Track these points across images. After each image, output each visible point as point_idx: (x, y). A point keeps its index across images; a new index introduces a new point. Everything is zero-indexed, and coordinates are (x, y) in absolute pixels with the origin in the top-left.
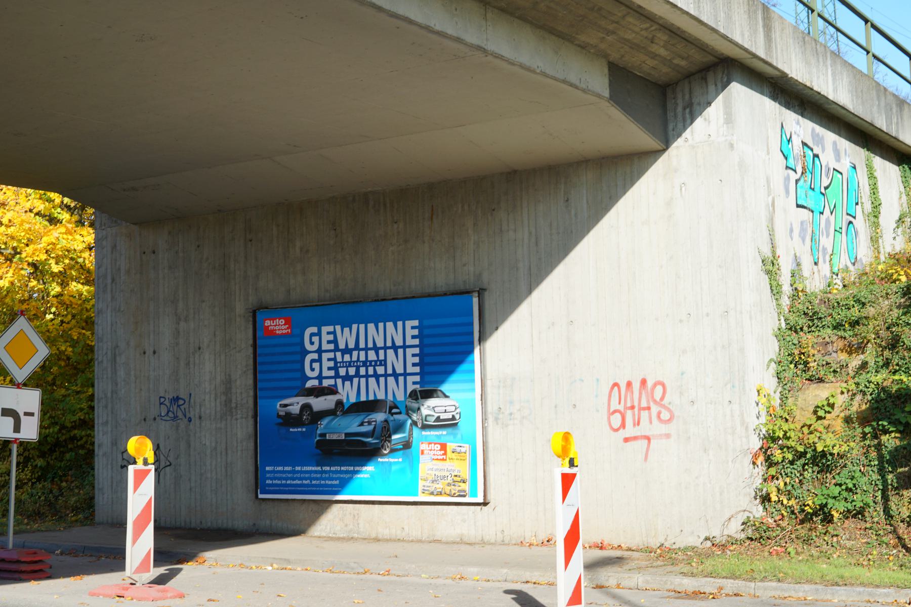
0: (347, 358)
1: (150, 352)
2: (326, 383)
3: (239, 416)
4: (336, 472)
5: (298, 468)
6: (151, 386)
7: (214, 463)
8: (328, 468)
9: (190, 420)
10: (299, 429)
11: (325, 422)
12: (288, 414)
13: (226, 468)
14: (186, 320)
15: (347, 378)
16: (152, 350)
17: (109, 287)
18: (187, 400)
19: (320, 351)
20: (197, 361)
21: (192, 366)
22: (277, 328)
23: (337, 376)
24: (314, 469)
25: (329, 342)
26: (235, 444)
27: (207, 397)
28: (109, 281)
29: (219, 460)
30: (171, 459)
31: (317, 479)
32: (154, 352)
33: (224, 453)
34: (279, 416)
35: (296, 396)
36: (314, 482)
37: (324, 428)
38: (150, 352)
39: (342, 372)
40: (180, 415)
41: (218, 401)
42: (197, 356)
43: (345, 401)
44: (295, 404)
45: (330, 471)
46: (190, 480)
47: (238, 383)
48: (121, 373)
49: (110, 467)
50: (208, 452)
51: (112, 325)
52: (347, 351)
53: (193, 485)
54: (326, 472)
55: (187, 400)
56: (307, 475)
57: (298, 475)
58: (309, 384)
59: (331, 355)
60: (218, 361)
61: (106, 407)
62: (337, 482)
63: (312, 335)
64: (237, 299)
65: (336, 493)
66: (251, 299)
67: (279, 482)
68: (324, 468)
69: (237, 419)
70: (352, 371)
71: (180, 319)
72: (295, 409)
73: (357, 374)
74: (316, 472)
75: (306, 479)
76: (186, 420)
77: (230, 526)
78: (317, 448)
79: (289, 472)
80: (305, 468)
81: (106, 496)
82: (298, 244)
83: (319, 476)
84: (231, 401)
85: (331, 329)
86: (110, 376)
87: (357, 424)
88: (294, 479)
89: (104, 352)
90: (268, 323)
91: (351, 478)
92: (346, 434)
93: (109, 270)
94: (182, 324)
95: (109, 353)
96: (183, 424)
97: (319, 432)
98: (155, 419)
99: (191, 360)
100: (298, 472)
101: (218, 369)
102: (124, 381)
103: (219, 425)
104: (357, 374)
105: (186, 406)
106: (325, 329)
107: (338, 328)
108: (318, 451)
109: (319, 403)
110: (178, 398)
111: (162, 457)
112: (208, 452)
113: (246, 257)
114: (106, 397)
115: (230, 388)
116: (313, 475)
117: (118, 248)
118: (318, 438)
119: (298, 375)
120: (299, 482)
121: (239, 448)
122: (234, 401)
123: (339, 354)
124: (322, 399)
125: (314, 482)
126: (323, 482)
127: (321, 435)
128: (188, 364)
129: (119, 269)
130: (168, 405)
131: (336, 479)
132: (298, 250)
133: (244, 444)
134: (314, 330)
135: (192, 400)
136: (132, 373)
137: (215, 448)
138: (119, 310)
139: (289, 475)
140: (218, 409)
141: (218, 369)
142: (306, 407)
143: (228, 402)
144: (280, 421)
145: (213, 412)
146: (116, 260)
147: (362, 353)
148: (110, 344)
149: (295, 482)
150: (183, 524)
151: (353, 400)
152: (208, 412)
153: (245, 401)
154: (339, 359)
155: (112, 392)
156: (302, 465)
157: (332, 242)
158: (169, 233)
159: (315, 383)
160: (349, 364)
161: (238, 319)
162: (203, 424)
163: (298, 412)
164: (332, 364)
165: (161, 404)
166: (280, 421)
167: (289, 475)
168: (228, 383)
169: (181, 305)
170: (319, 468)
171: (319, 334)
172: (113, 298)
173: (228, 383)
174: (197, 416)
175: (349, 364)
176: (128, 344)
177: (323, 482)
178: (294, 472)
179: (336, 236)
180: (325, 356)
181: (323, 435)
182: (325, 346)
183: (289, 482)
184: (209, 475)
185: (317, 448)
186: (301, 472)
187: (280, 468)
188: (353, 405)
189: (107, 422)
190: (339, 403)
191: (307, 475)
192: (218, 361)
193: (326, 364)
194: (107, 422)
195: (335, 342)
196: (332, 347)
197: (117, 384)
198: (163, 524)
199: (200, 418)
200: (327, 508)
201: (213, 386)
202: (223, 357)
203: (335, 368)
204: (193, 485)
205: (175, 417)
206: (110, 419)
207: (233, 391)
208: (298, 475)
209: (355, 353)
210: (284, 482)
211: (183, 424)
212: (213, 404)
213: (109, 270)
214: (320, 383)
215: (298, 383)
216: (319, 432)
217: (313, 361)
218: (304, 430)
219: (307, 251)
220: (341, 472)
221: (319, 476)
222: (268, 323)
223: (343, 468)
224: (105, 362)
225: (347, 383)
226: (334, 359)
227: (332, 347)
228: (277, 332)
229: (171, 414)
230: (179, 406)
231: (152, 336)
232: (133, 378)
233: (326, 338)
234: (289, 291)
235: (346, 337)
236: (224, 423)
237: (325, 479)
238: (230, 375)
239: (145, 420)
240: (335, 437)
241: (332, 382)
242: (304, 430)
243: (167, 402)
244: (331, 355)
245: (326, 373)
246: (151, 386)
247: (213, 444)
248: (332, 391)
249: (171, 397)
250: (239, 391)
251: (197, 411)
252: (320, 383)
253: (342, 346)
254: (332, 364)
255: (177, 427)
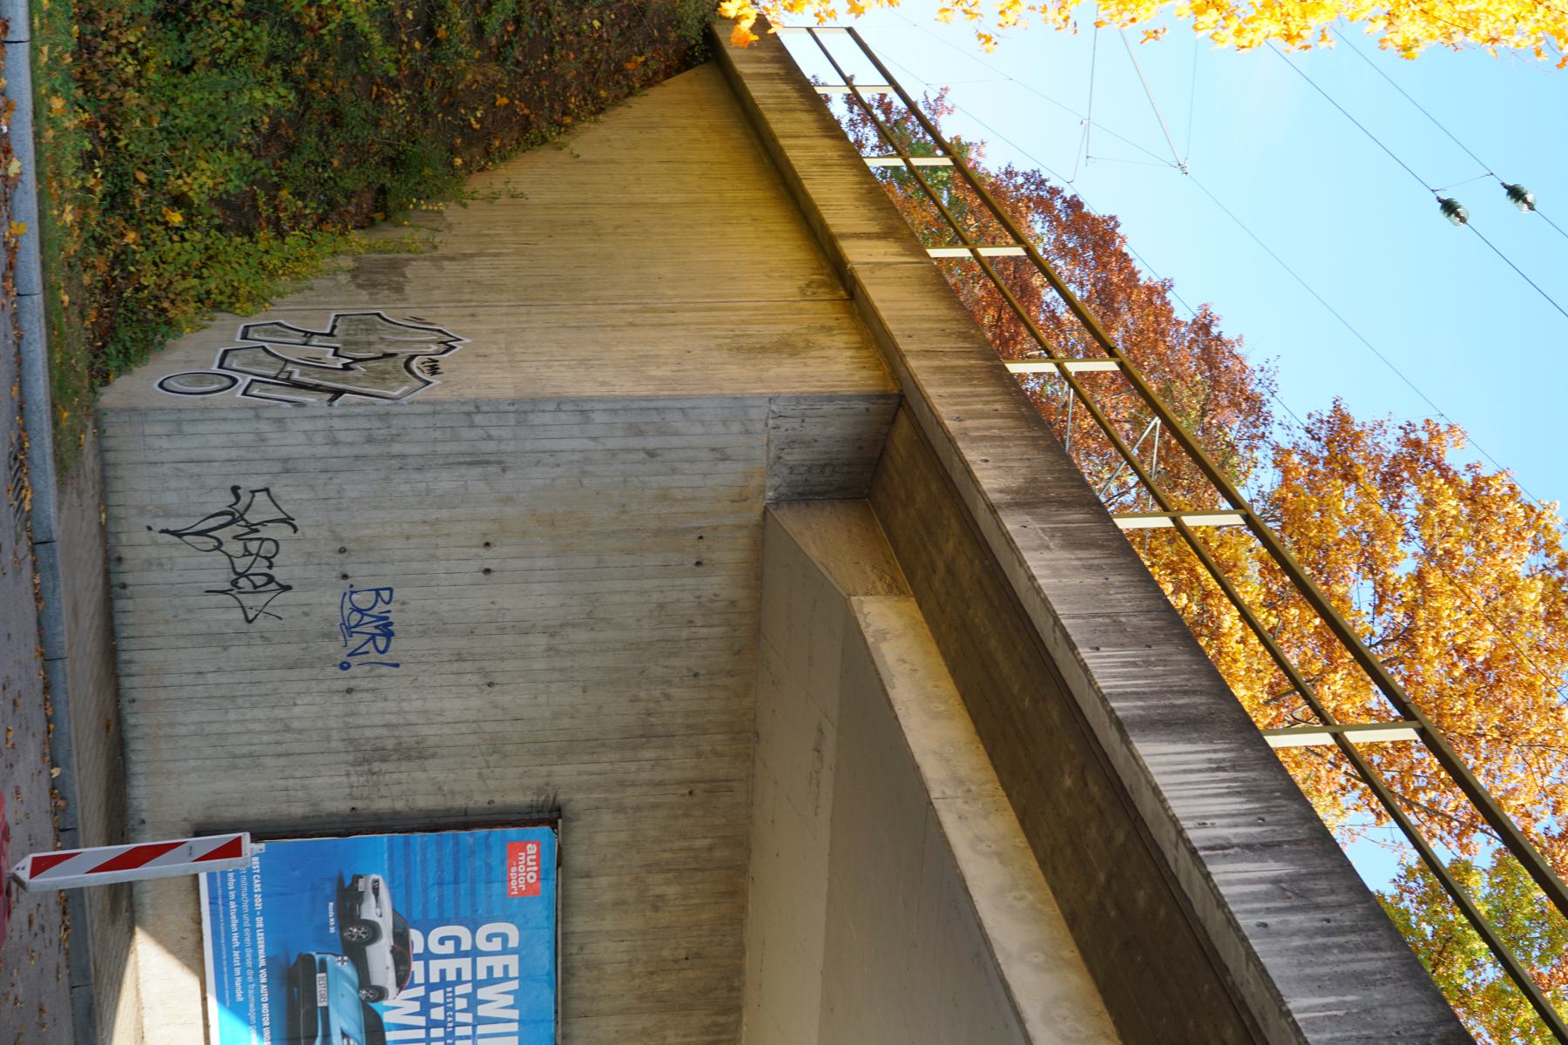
0: (461, 1003)
1: (490, 558)
2: (417, 967)
3: (353, 779)
4: (258, 996)
5: (260, 922)
6: (415, 565)
7: (258, 727)
8: (263, 980)
9: (345, 666)
10: (331, 914)
11: (348, 968)
12: (359, 897)
13: (250, 755)
14: (551, 650)
15: (426, 1005)
16: (482, 551)
17: (635, 442)
18: (384, 658)
19: (474, 953)
20: (465, 679)
21: (455, 667)
22: (522, 868)
23: (430, 987)
24: (261, 952)
25: (490, 969)
26: (298, 774)
27: (392, 706)
28: (652, 442)
29: (265, 738)
30: (261, 622)
31: (243, 960)
32: (487, 571)
33: (280, 749)
34: (356, 878)
35: (394, 912)
36: (236, 954)
37: (337, 969)
38: (490, 558)
39: (437, 996)
40: (356, 641)
41: (384, 732)
42: (476, 679)
43: (385, 1003)
44: (378, 911)
45: (258, 984)
46: (219, 670)
47: (420, 775)
48: (446, 482)
49: (234, 453)
50: (280, 713)
51: (553, 453)
52: (473, 1002)
53: (210, 678)
54: (256, 975)
55: (384, 658)
56: (248, 940)
57: (247, 923)
58: (415, 936)
59: (467, 976)
60: (463, 728)
61: (370, 440)
62: (239, 998)
63: (505, 938)
64: (583, 767)
65: (220, 998)
66: (580, 796)
67: (234, 926)
68: (263, 972)
69: (348, 775)
70: (437, 1014)
71: (552, 636)
72: (369, 911)
73: (432, 1024)
74: (255, 956)
75: (241, 939)
76: (342, 657)
77: (135, 769)
78: (300, 956)
79: (252, 904)
80: (260, 936)
81: (165, 443)
82: (671, 891)
83: (249, 963)
84: (384, 760)
85: (514, 972)
86: (440, 448)
87: (346, 1028)
88: (239, 914)
89: (494, 432)
90: (532, 849)
91: (248, 1022)
92: (326, 1009)
93: (675, 441)
94: (541, 641)
95: (491, 446)
96: (336, 650)
97: (329, 958)
98: (345, 577)
99: (467, 666)
100: (253, 922)
101: (447, 730)
102: (428, 492)
103: (335, 734)
104: (432, 1024)
105: (374, 656)
106: (513, 962)
107: (514, 985)
108: (293, 960)
109: (380, 956)
110: (389, 635)
111: (264, 598)
112: (280, 713)
113: (660, 783)
114: (394, 438)
115: (409, 758)
116: (249, 952)
117: (721, 466)
118: (317, 958)
119: (433, 914)
120: (234, 926)
121: (291, 782)
122: (385, 766)
123: (467, 988)
124: (389, 960)
125: (236, 954)
126: (238, 971)
127: (323, 962)
128: (460, 658)
129: (674, 471)
130: (375, 611)
131: (245, 995)
132: (659, 891)
133: (300, 794)
134: (514, 942)
135: (385, 670)
136: (445, 514)
137: (288, 729)
138: (584, 473)
139: (245, 906)
140: (368, 733)
141: (447, 730)
142: (373, 932)
143: (381, 754)
144: (348, 883)
145: (360, 721)
146: (693, 461)
147: (468, 1031)
148: (510, 447)
149: (233, 917)
150: (124, 656)
151: (388, 1018)
152: (362, 708)
153: (384, 791)
154: (460, 990)
155: (403, 456)
156: (266, 930)
157: (665, 953)
158: (733, 603)
159: (418, 948)
160: (449, 1008)
161: (544, 770)
162: (336, 698)
163: (364, 917)
164: (451, 976)
165: (377, 591)
166: (348, 883)
167: (245, 906)
168: (415, 753)
169: (582, 636)
170: (262, 963)
171: (505, 951)
172: (613, 453)
173: (415, 753)
174: (352, 683)
175: (449, 1008)
176: (507, 500)
177: (238, 971)
178: (253, 914)
179: (676, 961)
180: (465, 964)
181: (323, 967)
182: (482, 963)
183: (233, 905)
184: (232, 716)
185: (300, 956)
186: (254, 929)
187: (257, 887)
188: (378, 1019)
189: (335, 443)
190: (381, 993)
191: (248, 940)
192: (463, 728)
193: (451, 966)
194: (335, 443)
195: (491, 980)
196: (482, 975)
197: (419, 469)
198: (136, 890)
199: (349, 691)
200: (189, 966)
201: (412, 718)
202: (472, 739)
203: (443, 984)
204: (210, 678)
205: (349, 630)
206: (345, 451)
207: (405, 765)
208: (247, 923)
209: (468, 1018)
210: (232, 895)
211: (336, 650)
212: (377, 720)
213: (675, 441)
214: (418, 957)
215: (417, 913)
216: (329, 958)
217: (457, 940)
218: (332, 930)
219: (656, 909)
220: (258, 1004)
221: (249, 963)
222: (532, 849)
223: (265, 1006)
224: (473, 434)
225: (416, 1006)
226: (459, 981)
227: (482, 975)
228: (514, 869)
229: (356, 617)
230: (373, 637)
231: (522, 564)
232: (434, 514)
233: (497, 963)
234: (588, 875)
235: (497, 1001)
236: (340, 746)
237: (243, 975)
238: (434, 756)
239: (342, 551)
240: (321, 989)
241: (419, 977)
242: (332, 930)
243: (380, 608)
244: (467, 976)
245: (435, 966)
246: (415, 565)
247: (296, 724)
248: (403, 980)
249: (392, 617)
250: (404, 777)
251: (364, 684)
252: (418, 957)
253: (482, 993)
254: (451, 976)
255: (327, 636)
